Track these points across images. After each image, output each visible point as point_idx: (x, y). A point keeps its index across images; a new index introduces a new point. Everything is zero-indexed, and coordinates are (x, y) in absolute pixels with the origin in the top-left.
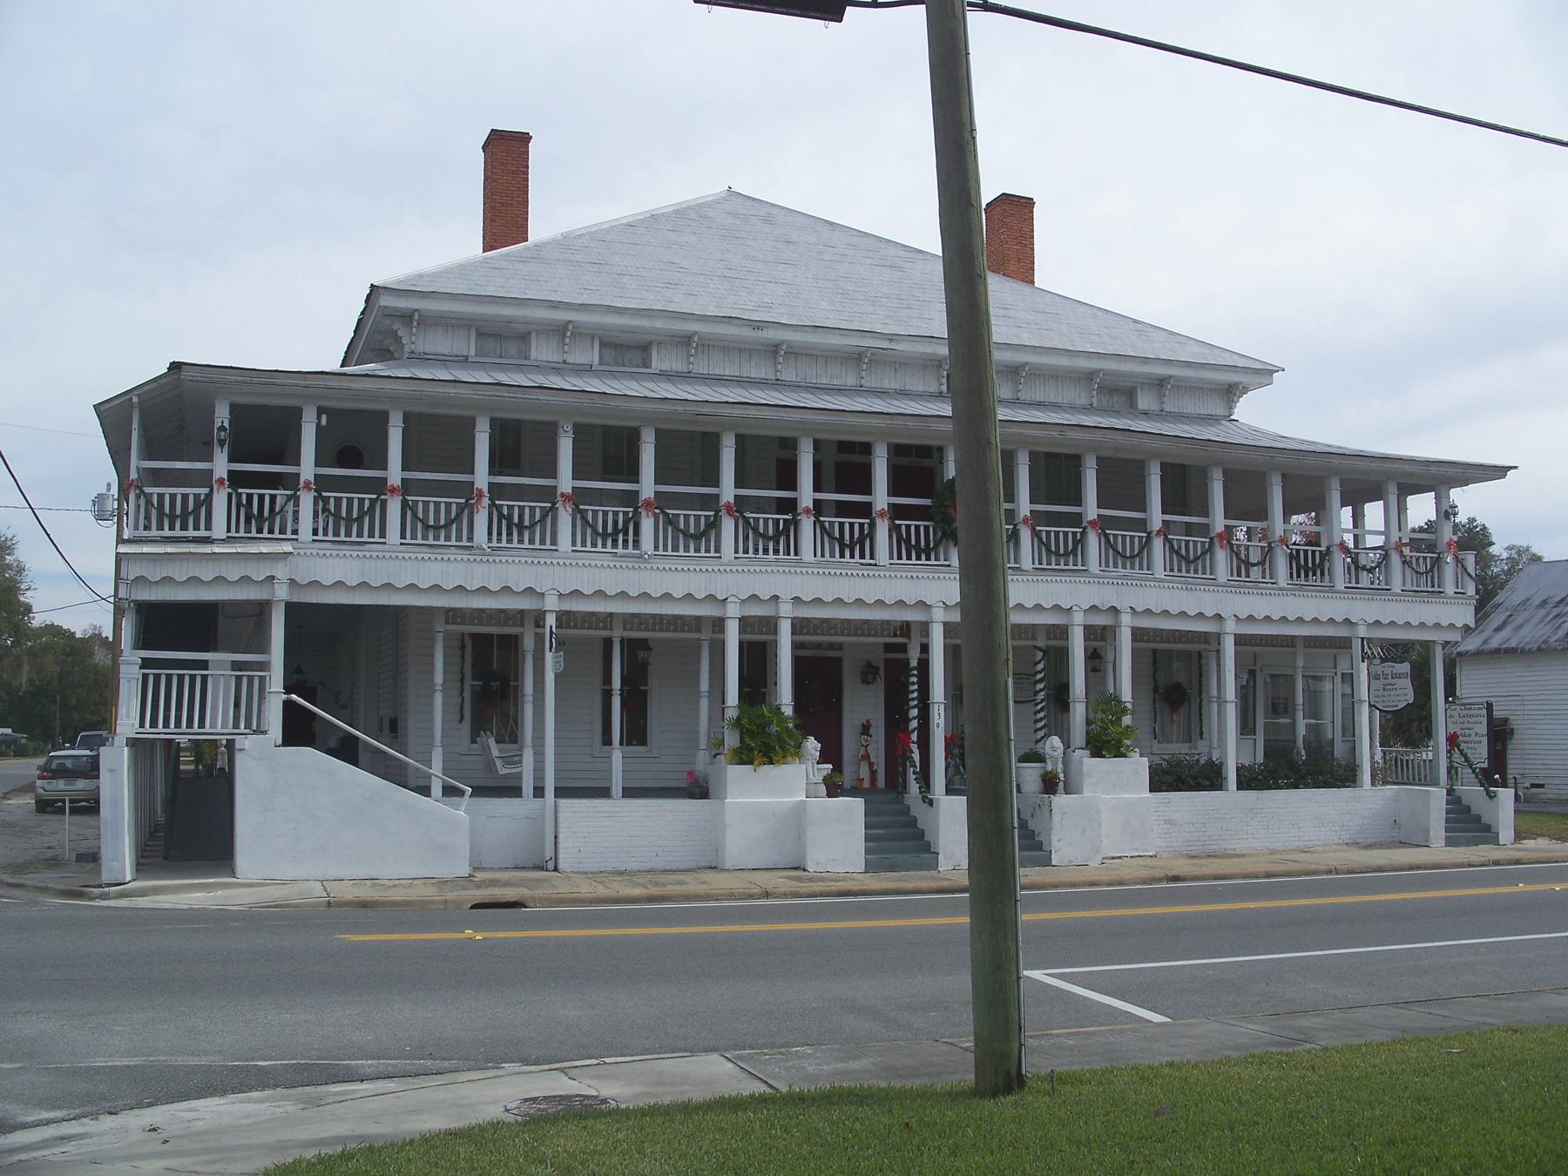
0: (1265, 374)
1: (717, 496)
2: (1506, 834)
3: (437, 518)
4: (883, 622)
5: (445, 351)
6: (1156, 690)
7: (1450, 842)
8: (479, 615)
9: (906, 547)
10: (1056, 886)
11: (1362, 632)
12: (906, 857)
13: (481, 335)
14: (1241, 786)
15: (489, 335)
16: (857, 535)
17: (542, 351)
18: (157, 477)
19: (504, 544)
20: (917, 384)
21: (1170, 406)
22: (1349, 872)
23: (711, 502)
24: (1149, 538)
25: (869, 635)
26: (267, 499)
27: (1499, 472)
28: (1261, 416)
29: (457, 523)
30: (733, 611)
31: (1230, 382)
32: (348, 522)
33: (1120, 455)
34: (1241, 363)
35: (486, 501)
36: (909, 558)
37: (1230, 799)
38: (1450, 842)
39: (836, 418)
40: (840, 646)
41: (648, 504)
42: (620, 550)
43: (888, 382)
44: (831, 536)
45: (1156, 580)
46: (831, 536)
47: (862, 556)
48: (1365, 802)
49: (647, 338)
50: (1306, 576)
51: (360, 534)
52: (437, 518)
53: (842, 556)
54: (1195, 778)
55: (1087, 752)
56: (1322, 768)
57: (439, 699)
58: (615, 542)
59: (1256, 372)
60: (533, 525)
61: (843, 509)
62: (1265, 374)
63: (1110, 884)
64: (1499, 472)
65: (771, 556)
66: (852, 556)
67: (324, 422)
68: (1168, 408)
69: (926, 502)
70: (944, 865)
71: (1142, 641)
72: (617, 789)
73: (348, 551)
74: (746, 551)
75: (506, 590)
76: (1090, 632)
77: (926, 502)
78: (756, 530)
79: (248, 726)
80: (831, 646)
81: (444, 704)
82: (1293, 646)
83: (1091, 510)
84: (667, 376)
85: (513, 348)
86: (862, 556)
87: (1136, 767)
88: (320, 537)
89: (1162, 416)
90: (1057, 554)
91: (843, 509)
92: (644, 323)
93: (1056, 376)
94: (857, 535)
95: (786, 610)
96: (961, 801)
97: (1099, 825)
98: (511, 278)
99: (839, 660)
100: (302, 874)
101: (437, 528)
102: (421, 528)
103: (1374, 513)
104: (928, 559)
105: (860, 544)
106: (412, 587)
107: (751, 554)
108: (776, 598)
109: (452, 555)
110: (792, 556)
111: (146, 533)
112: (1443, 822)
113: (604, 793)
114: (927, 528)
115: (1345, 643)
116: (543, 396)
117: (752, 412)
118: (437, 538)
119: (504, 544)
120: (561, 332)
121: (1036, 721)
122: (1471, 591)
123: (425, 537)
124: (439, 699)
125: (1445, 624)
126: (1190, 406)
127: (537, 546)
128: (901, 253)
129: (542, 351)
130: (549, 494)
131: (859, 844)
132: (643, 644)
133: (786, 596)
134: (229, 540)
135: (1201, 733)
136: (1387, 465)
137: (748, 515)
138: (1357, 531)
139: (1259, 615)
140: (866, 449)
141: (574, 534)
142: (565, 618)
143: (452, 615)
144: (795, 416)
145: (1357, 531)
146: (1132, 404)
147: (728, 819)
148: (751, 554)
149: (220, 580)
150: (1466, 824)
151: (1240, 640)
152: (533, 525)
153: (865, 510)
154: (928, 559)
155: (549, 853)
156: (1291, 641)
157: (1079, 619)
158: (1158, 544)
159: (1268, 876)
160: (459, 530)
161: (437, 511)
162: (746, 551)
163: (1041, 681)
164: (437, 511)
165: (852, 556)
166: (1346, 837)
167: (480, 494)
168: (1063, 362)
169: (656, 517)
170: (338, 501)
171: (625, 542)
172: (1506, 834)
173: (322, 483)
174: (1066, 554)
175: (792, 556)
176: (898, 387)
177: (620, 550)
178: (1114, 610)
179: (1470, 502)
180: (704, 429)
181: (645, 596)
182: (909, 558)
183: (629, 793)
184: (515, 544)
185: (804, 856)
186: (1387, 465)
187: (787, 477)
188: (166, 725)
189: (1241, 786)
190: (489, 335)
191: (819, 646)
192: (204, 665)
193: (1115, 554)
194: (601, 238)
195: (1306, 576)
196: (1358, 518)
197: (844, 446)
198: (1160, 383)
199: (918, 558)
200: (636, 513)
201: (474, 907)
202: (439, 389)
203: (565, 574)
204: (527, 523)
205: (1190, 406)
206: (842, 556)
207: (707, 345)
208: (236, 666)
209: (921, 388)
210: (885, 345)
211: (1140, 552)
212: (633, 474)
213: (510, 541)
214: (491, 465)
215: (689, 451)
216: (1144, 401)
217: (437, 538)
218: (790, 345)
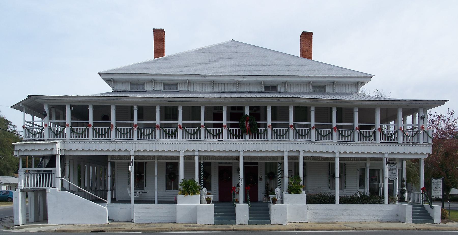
0: (369, 77)
1: (289, 124)
2: (437, 219)
3: (146, 133)
4: (219, 156)
5: (122, 89)
6: (329, 174)
7: (413, 222)
8: (166, 157)
9: (233, 135)
10: (258, 230)
11: (386, 156)
12: (226, 220)
13: (132, 84)
14: (340, 202)
15: (134, 84)
16: (218, 132)
17: (148, 87)
18: (166, 125)
19: (120, 138)
20: (255, 89)
21: (336, 90)
22: (360, 230)
23: (331, 126)
24: (310, 130)
25: (215, 160)
26: (215, 130)
27: (442, 102)
28: (368, 91)
29: (350, 136)
30: (182, 154)
31: (359, 80)
32: (324, 136)
33: (325, 106)
34: (359, 75)
35: (114, 128)
36: (233, 138)
37: (337, 206)
38: (413, 222)
39: (208, 100)
40: (232, 163)
41: (335, 128)
42: (151, 139)
43: (246, 89)
44: (211, 134)
45: (291, 141)
46: (211, 134)
47: (219, 138)
48: (386, 209)
49: (176, 82)
50: (169, 137)
51: (286, 138)
52: (146, 133)
53: (214, 138)
54: (324, 200)
55: (288, 192)
56: (374, 197)
57: (156, 179)
58: (172, 137)
59: (365, 77)
60: (127, 133)
61: (215, 125)
62: (369, 77)
63: (276, 230)
64: (442, 102)
65: (193, 139)
66: (216, 138)
67: (72, 109)
68: (336, 91)
69: (238, 122)
70: (237, 223)
71: (291, 160)
72: (156, 201)
73: (79, 142)
74: (186, 138)
75: (120, 150)
76: (290, 158)
77: (238, 122)
78: (188, 132)
79: (51, 186)
80: (229, 163)
81: (158, 180)
82: (366, 160)
83: (313, 123)
84: (181, 92)
85: (175, 87)
86: (219, 138)
87: (303, 195)
88: (72, 138)
89: (334, 93)
90: (302, 136)
91: (215, 125)
92: (172, 78)
93: (299, 84)
94: (218, 132)
95: (338, 155)
96: (247, 206)
97: (286, 213)
98: (162, 68)
99: (231, 167)
100: (64, 223)
101: (147, 135)
102: (98, 135)
103: (409, 119)
104: (239, 138)
105: (219, 135)
106: (95, 150)
107: (187, 139)
108: (194, 150)
109: (105, 141)
110: (199, 139)
111: (28, 139)
112: (411, 216)
113: (153, 202)
114: (239, 130)
115: (381, 159)
116: (125, 99)
117: (183, 100)
118: (283, 138)
119: (120, 138)
120: (154, 82)
121: (280, 185)
122: (430, 141)
123: (99, 137)
124: (156, 179)
125: (117, 150)
126: (344, 90)
127: (128, 138)
128: (271, 53)
129: (148, 87)
130: (287, 125)
131: (213, 217)
132: (114, 162)
133: (197, 150)
134: (49, 140)
135: (345, 187)
136: (395, 103)
137: (186, 128)
138: (404, 125)
139: (68, 149)
140: (221, 108)
141: (315, 136)
142: (136, 157)
143: (159, 158)
144: (196, 100)
145: (404, 125)
146: (325, 91)
147: (177, 210)
148: (187, 139)
149: (33, 150)
150: (422, 215)
151: (340, 159)
152: (127, 133)
153: (308, 126)
154: (239, 138)
155: (132, 218)
156: (365, 159)
157: (286, 154)
158: (313, 131)
159: (330, 230)
160: (286, 136)
161: (147, 131)
162: (186, 138)
163: (279, 172)
164: (147, 131)
165: (216, 138)
166: (379, 219)
167: (90, 126)
168: (298, 79)
169: (160, 130)
170: (121, 129)
171: (175, 137)
172: (437, 219)
173: (273, 125)
174: (102, 135)
175: (199, 139)
176: (249, 91)
177: (151, 139)
178: (298, 151)
179: (432, 113)
180: (165, 105)
181: (157, 151)
182: (233, 138)
183: (160, 202)
184: (123, 138)
185: (197, 220)
186: (395, 103)
187: (108, 117)
188: (40, 186)
189: (340, 202)
190: (134, 84)
191: (226, 163)
192: (51, 171)
193: (298, 135)
194: (178, 56)
195: (169, 137)
196: (405, 120)
197: (215, 108)
198: (333, 83)
199: (236, 138)
200: (332, 130)
201: (91, 232)
202: (187, 100)
203: (181, 146)
204: (368, 135)
205: (344, 90)
206: (214, 138)
207: (340, 84)
208: (44, 171)
209: (256, 91)
210: (242, 79)
211: (286, 133)
212: (177, 119)
213: (141, 138)
214: (160, 119)
215: (192, 112)
216: (328, 89)
217: (283, 138)
218: (337, 82)
